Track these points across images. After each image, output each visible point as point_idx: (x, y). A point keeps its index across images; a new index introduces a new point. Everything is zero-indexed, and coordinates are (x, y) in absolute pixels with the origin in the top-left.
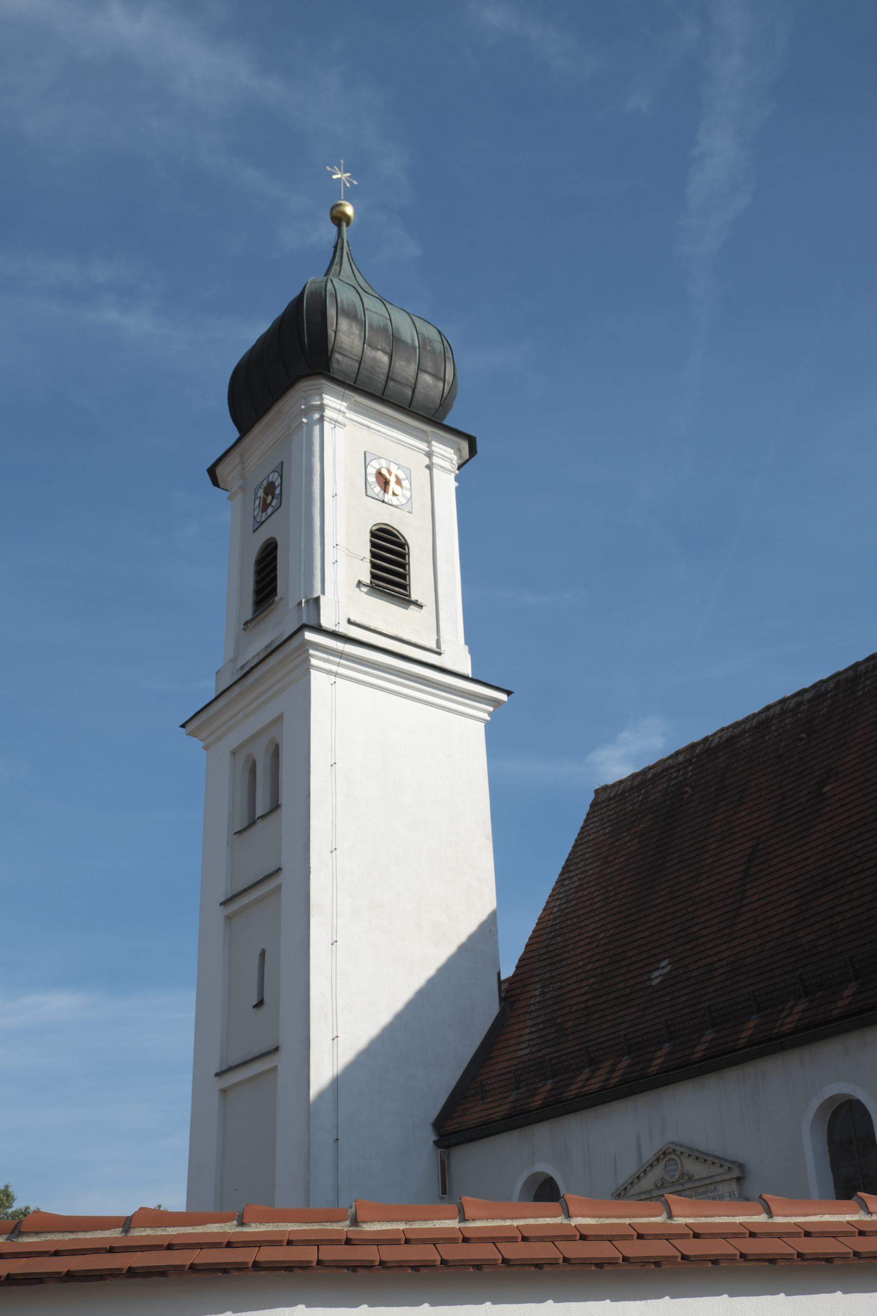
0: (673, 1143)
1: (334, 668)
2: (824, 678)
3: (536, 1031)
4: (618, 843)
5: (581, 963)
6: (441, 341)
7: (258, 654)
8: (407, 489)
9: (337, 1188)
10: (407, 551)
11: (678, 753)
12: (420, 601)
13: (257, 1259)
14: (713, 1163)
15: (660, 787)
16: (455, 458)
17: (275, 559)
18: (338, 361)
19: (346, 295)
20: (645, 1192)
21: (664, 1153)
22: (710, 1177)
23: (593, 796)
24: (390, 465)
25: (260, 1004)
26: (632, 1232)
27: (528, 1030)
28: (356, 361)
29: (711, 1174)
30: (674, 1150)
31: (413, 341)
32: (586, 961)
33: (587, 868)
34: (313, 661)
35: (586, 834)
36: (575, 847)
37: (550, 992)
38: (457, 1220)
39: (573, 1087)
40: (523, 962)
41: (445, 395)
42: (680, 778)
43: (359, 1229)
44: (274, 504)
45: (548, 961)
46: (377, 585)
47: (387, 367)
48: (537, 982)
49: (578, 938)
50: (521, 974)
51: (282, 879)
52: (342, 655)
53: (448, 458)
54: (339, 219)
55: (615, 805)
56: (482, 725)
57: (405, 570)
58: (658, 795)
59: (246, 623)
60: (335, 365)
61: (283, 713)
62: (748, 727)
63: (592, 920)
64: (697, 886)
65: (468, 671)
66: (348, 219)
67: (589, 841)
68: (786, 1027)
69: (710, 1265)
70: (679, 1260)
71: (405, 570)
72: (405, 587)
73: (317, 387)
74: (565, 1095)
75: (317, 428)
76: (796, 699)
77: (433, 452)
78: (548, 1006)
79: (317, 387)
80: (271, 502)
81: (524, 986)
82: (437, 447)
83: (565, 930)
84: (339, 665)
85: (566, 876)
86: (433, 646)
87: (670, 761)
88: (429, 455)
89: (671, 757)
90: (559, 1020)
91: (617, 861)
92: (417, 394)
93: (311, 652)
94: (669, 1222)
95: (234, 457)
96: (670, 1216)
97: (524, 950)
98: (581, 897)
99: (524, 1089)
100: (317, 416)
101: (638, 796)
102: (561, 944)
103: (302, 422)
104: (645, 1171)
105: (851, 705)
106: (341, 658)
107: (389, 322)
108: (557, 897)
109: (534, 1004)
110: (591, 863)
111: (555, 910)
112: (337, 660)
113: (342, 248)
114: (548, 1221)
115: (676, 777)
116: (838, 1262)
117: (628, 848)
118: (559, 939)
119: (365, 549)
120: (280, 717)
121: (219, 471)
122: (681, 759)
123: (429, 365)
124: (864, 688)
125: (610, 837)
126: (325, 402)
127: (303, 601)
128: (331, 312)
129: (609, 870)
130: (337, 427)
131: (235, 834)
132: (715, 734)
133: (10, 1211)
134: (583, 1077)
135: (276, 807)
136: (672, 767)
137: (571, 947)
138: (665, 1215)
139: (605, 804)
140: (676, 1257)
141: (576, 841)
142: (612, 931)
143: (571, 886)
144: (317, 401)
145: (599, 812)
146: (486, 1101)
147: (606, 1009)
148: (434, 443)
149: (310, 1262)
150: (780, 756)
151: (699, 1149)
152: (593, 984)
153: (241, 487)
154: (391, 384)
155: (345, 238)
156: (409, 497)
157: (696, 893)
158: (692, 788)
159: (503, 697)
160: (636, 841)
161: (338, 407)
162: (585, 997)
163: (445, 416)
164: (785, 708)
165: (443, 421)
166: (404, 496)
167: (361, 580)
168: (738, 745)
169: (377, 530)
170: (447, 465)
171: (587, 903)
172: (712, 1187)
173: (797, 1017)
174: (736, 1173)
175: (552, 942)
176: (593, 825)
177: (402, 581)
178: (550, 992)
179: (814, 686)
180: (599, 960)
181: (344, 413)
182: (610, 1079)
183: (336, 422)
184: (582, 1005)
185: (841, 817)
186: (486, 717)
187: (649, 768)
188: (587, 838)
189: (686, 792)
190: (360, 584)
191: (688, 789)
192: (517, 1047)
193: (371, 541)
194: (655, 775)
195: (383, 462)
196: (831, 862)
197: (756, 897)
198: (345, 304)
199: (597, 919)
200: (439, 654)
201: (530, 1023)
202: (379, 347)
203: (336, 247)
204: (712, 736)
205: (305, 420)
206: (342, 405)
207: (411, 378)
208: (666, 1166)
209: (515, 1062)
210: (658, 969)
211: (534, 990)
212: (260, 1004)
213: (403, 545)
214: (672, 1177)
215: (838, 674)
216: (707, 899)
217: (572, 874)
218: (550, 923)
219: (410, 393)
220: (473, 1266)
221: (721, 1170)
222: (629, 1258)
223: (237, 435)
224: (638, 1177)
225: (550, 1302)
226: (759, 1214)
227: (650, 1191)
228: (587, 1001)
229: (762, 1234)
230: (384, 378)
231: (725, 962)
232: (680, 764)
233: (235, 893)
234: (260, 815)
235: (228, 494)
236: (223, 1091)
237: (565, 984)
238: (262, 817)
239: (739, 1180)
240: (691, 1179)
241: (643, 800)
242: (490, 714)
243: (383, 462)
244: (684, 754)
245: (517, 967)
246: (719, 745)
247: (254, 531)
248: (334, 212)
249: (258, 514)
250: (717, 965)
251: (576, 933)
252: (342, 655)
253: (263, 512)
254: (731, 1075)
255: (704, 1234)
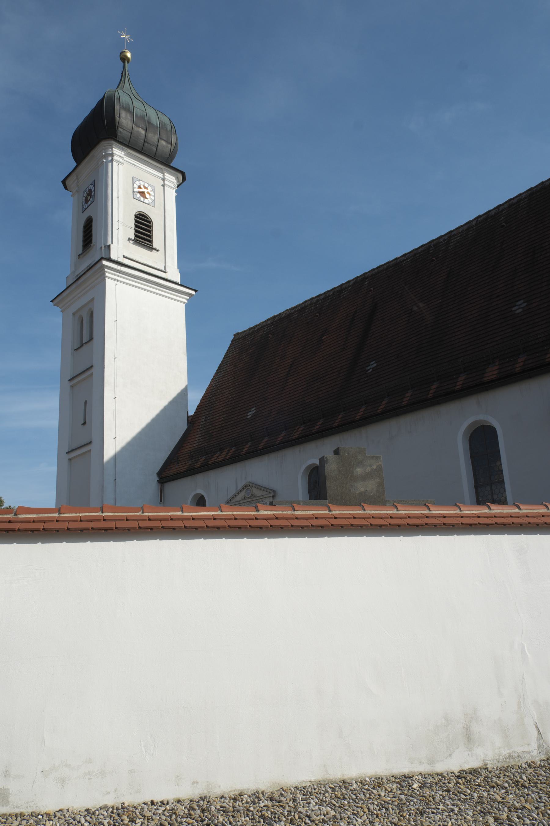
0: (250, 482)
1: (116, 278)
2: (329, 290)
3: (201, 436)
4: (241, 358)
5: (221, 408)
6: (170, 125)
7: (84, 270)
8: (152, 195)
9: (115, 499)
10: (152, 225)
11: (268, 320)
12: (157, 248)
13: (44, 528)
14: (264, 490)
15: (260, 334)
16: (175, 182)
17: (91, 226)
18: (120, 132)
19: (125, 99)
20: (238, 501)
21: (246, 486)
22: (263, 496)
23: (233, 337)
24: (144, 184)
25: (84, 423)
26: (313, 517)
27: (198, 436)
28: (130, 132)
29: (263, 494)
30: (250, 485)
31: (157, 124)
32: (224, 407)
33: (228, 368)
34: (107, 274)
35: (228, 353)
36: (224, 359)
37: (208, 420)
38: (58, 514)
39: (212, 459)
40: (199, 407)
41: (171, 151)
42: (268, 331)
43: (17, 517)
44: (91, 200)
45: (209, 407)
46: (137, 240)
47: (144, 136)
48: (204, 416)
49: (221, 398)
50: (198, 412)
51: (93, 370)
52: (120, 272)
53: (172, 182)
54: (124, 59)
55: (241, 341)
56: (184, 305)
57: (151, 234)
58: (259, 337)
59: (79, 255)
60: (119, 134)
61: (94, 297)
62: (297, 310)
63: (227, 390)
64: (269, 377)
65: (178, 280)
66: (128, 59)
67: (229, 356)
68: (294, 437)
69: (340, 528)
70: (330, 526)
71: (151, 234)
72: (151, 241)
73: (110, 144)
74: (209, 462)
75: (110, 164)
76: (317, 298)
77: (165, 178)
78: (207, 426)
79: (110, 144)
80: (90, 199)
81: (198, 417)
82: (168, 176)
83: (216, 394)
84: (119, 276)
85: (219, 371)
86: (163, 269)
87: (265, 323)
88: (164, 180)
89: (265, 321)
90: (210, 432)
91: (240, 365)
92: (158, 149)
93: (106, 270)
94: (142, 514)
95: (73, 177)
96: (143, 513)
97: (199, 402)
98: (224, 380)
99: (193, 460)
100: (110, 158)
101: (251, 338)
102: (214, 400)
103: (104, 161)
104: (238, 493)
105: (337, 302)
106: (119, 273)
107: (145, 114)
108: (215, 380)
109: (201, 425)
110: (229, 366)
111: (213, 385)
112: (118, 274)
113: (125, 74)
114: (94, 514)
115: (266, 330)
116: (199, 529)
117: (244, 360)
118: (214, 398)
119: (132, 224)
120: (93, 299)
121: (67, 182)
122: (269, 322)
123: (164, 136)
124: (344, 295)
125: (238, 355)
126: (114, 152)
127: (103, 246)
128: (117, 107)
129: (236, 369)
130: (119, 165)
131: (75, 350)
132: (284, 312)
133: (2, 507)
134: (216, 455)
135: (91, 339)
136: (265, 326)
137: (218, 401)
138: (141, 512)
139: (238, 340)
140: (329, 525)
141: (225, 356)
142: (234, 395)
143: (221, 376)
144: (110, 151)
145: (235, 344)
146: (179, 464)
147: (229, 427)
148: (166, 174)
149: (113, 528)
150: (308, 323)
151: (260, 485)
152: (225, 417)
153: (77, 191)
154: (146, 144)
155: (127, 69)
156: (153, 199)
157: (269, 380)
158: (272, 335)
159: (193, 293)
160: (248, 357)
161: (120, 154)
162: (222, 422)
163: (172, 161)
164: (312, 302)
165: (170, 164)
166: (151, 199)
167: (130, 237)
168: (292, 317)
169: (138, 214)
170: (172, 185)
171: (226, 383)
172: (263, 499)
173: (299, 433)
174: (272, 494)
175: (211, 399)
176: (232, 350)
177: (149, 239)
178: (208, 420)
179: (324, 293)
180: (229, 407)
181: (123, 158)
182: (227, 456)
183: (119, 162)
184: (220, 426)
185: (328, 350)
186: (186, 301)
187: (256, 326)
188: (229, 355)
189: (270, 337)
190: (129, 239)
191: (270, 335)
192: (194, 443)
193: (135, 220)
194: (258, 329)
195: (142, 183)
196: (321, 369)
197: (291, 383)
198: (124, 104)
199: (229, 390)
200: (165, 272)
201: (199, 433)
202: (140, 126)
203: (122, 74)
204: (282, 313)
205: (104, 160)
206: (122, 154)
207: (155, 142)
208: (246, 491)
209: (192, 449)
210: (251, 411)
211: (202, 419)
212: (84, 423)
213: (150, 222)
214: (248, 495)
215: (335, 288)
216: (272, 383)
217: (221, 370)
218: (211, 391)
219: (155, 149)
220: (80, 530)
221: (267, 493)
222: (230, 526)
223: (75, 164)
224: (236, 495)
225: (65, 542)
226: (178, 512)
227: (239, 501)
228: (222, 424)
229: (153, 519)
230: (143, 141)
231: (276, 409)
232: (268, 324)
233: (74, 376)
234: (85, 342)
235: (71, 193)
236: (70, 460)
237: (214, 417)
238: (86, 343)
239: (273, 497)
240: (255, 496)
241: (252, 339)
242: (187, 300)
243: (142, 183)
244: (271, 320)
245: (196, 409)
246: (285, 317)
247: (83, 212)
248: (121, 55)
249: (84, 204)
250: (273, 411)
251: (221, 395)
252: (120, 272)
253: (86, 204)
254: (273, 456)
255: (130, 519)
